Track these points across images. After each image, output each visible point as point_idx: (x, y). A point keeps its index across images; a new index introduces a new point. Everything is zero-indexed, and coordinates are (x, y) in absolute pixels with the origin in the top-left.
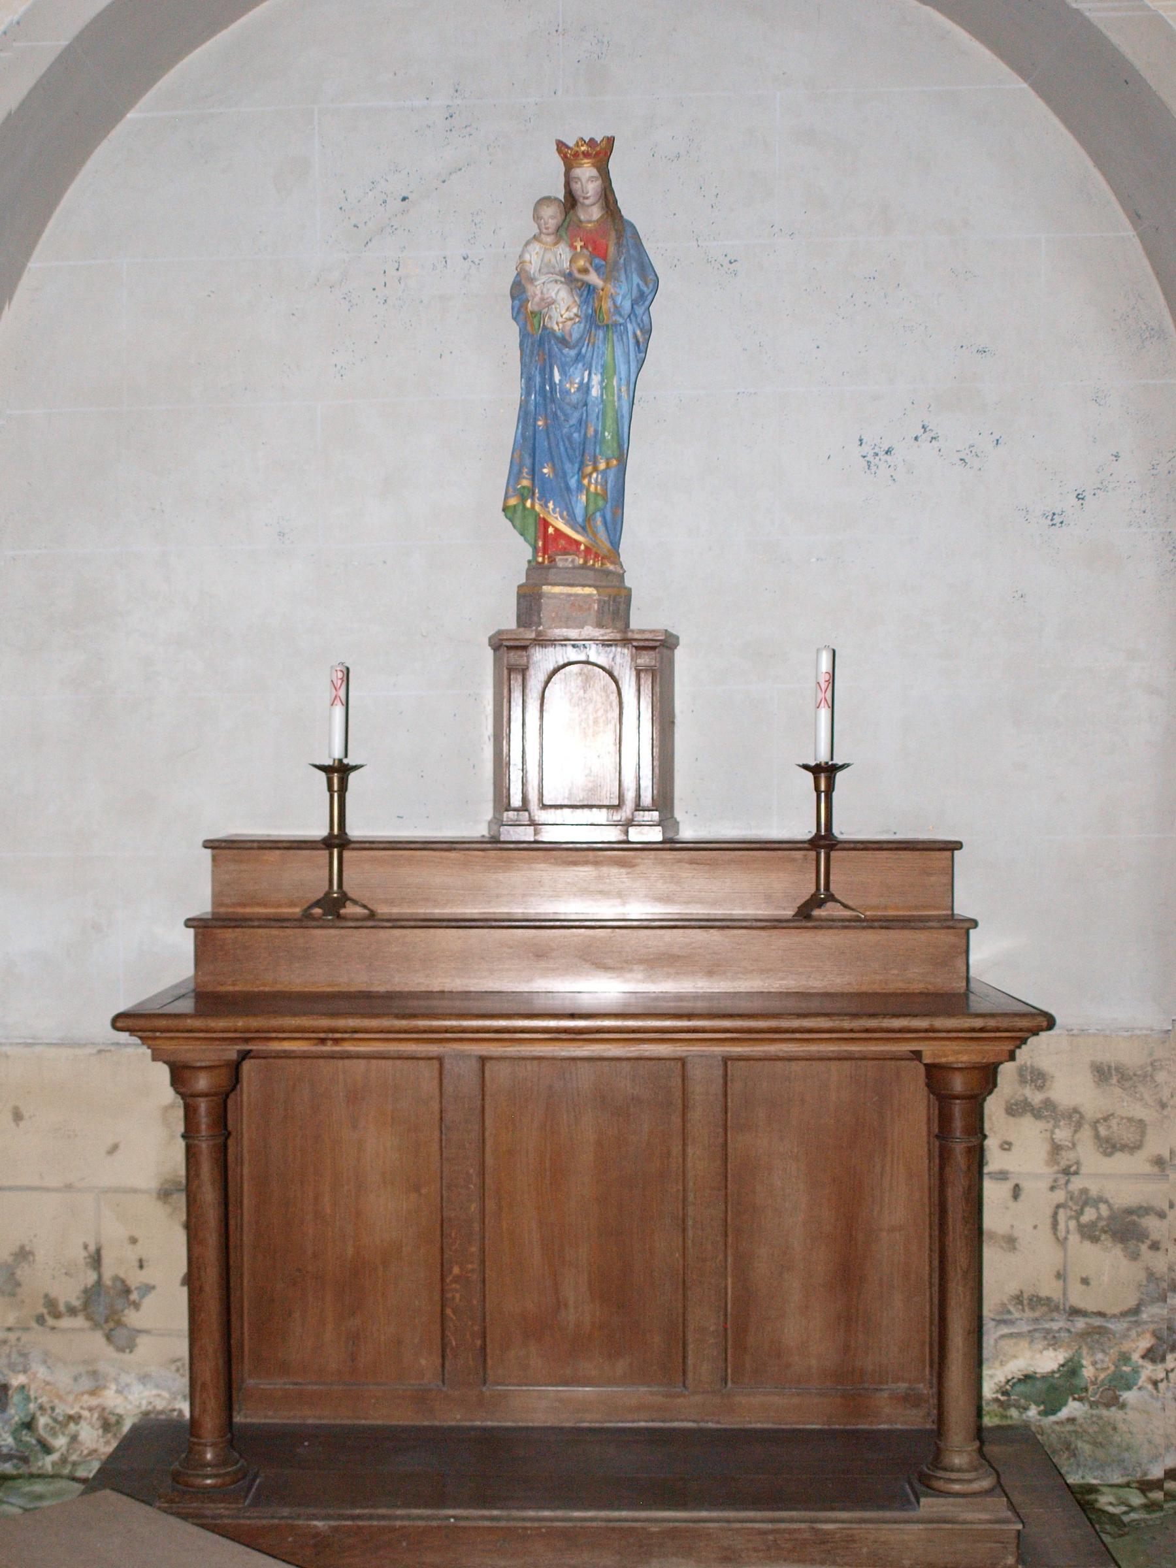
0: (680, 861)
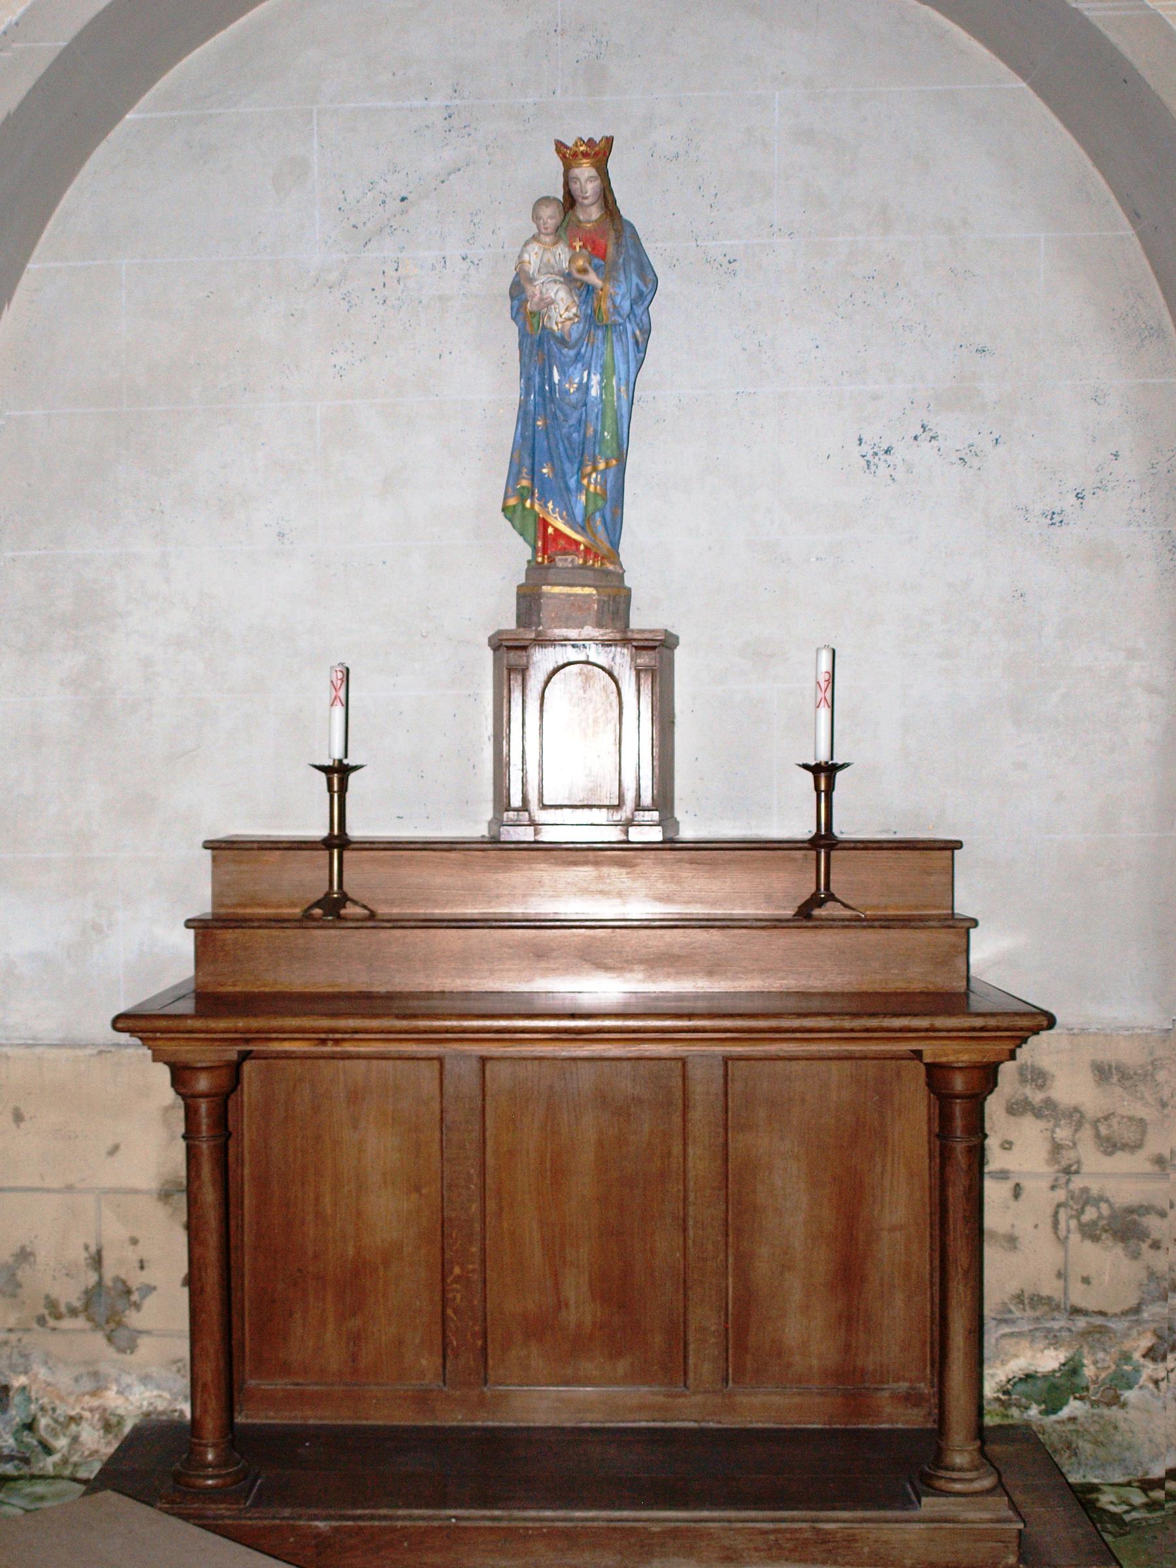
0: (680, 861)
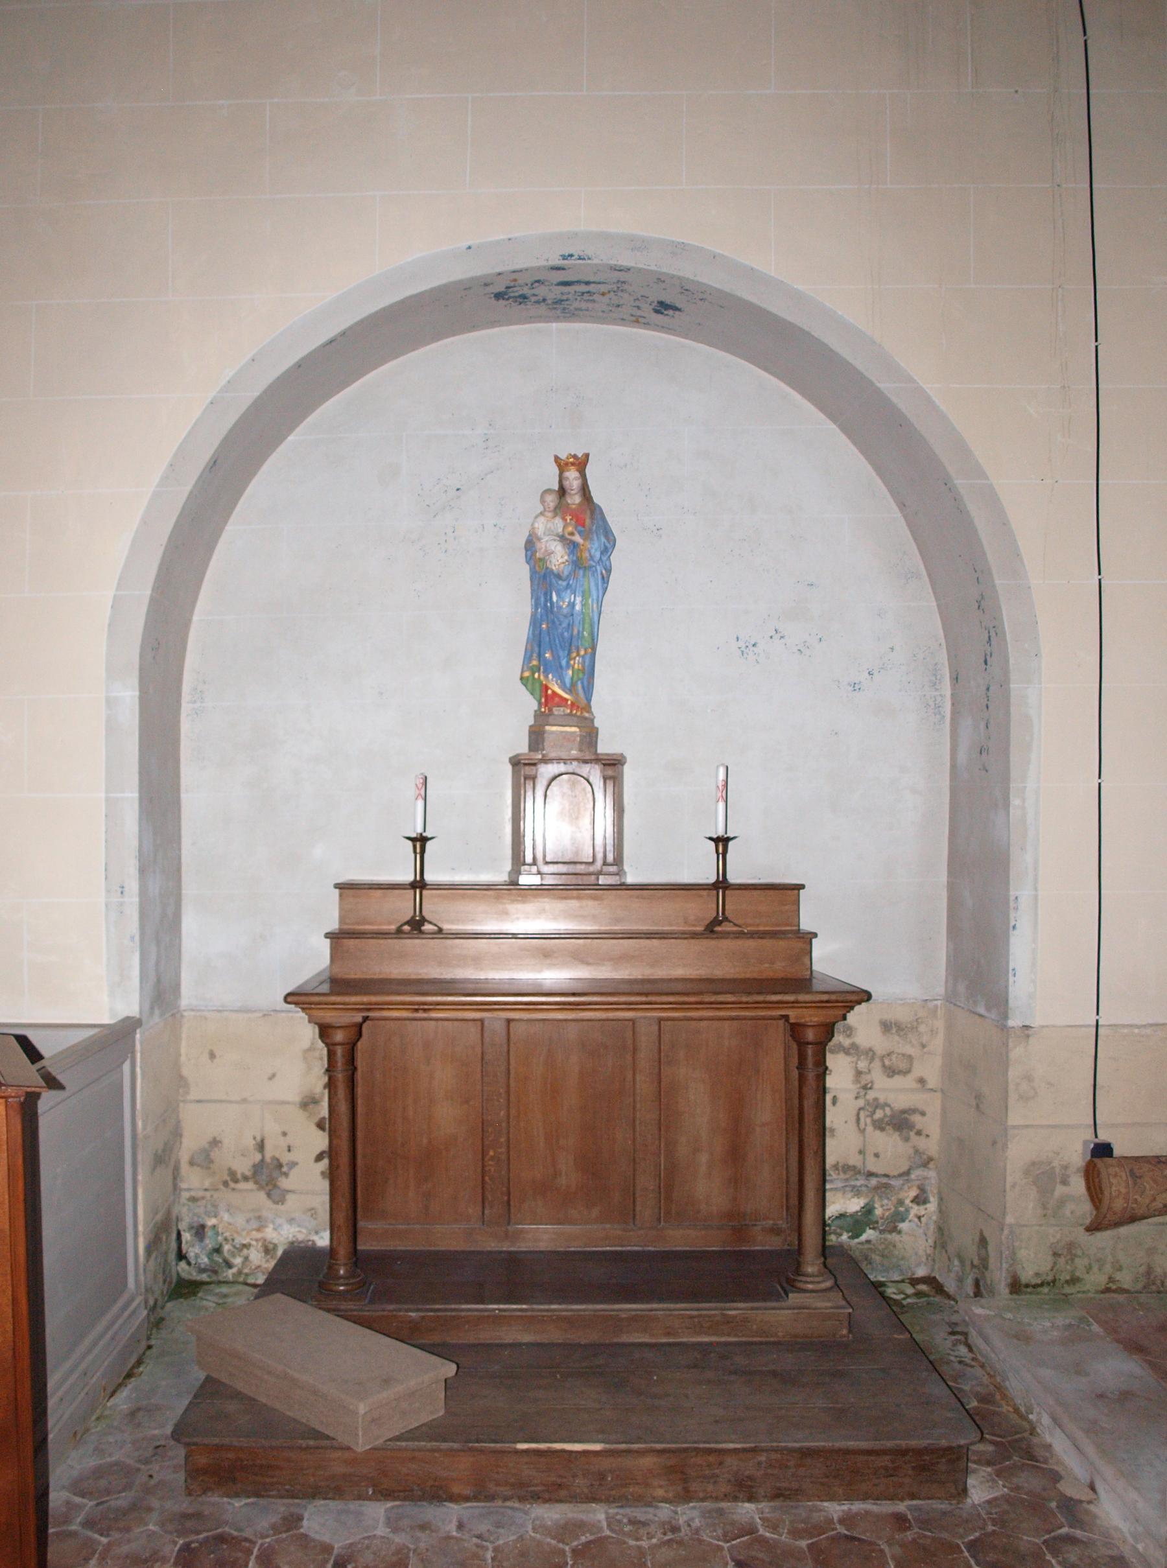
0: (631, 896)
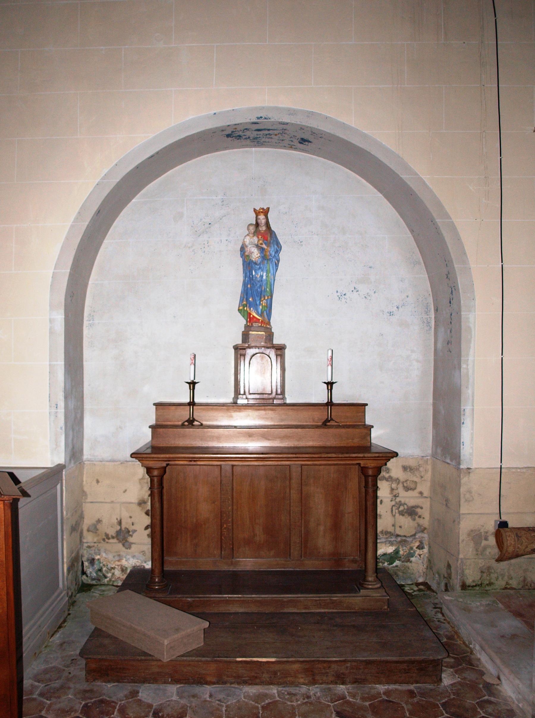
0: (289, 409)
